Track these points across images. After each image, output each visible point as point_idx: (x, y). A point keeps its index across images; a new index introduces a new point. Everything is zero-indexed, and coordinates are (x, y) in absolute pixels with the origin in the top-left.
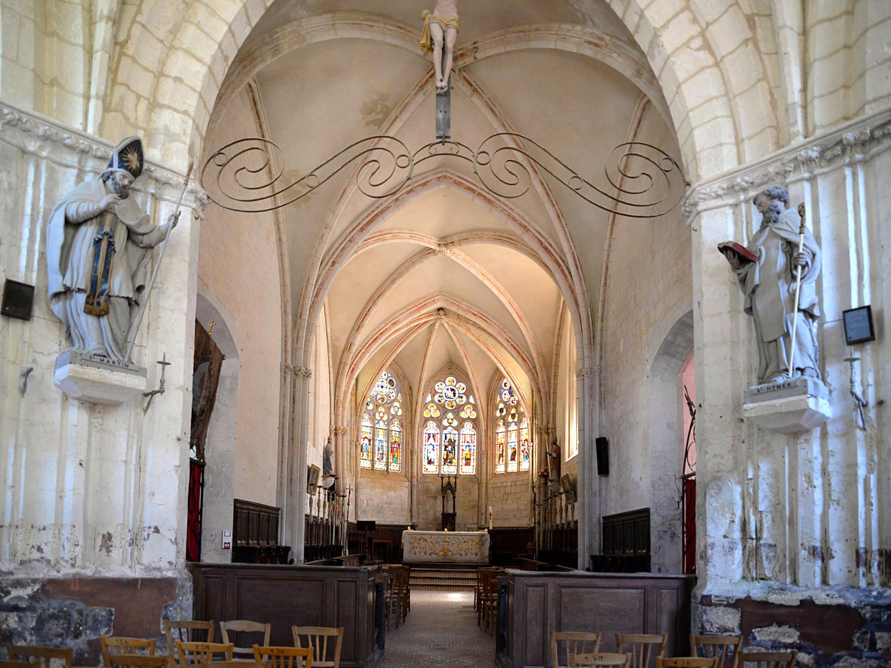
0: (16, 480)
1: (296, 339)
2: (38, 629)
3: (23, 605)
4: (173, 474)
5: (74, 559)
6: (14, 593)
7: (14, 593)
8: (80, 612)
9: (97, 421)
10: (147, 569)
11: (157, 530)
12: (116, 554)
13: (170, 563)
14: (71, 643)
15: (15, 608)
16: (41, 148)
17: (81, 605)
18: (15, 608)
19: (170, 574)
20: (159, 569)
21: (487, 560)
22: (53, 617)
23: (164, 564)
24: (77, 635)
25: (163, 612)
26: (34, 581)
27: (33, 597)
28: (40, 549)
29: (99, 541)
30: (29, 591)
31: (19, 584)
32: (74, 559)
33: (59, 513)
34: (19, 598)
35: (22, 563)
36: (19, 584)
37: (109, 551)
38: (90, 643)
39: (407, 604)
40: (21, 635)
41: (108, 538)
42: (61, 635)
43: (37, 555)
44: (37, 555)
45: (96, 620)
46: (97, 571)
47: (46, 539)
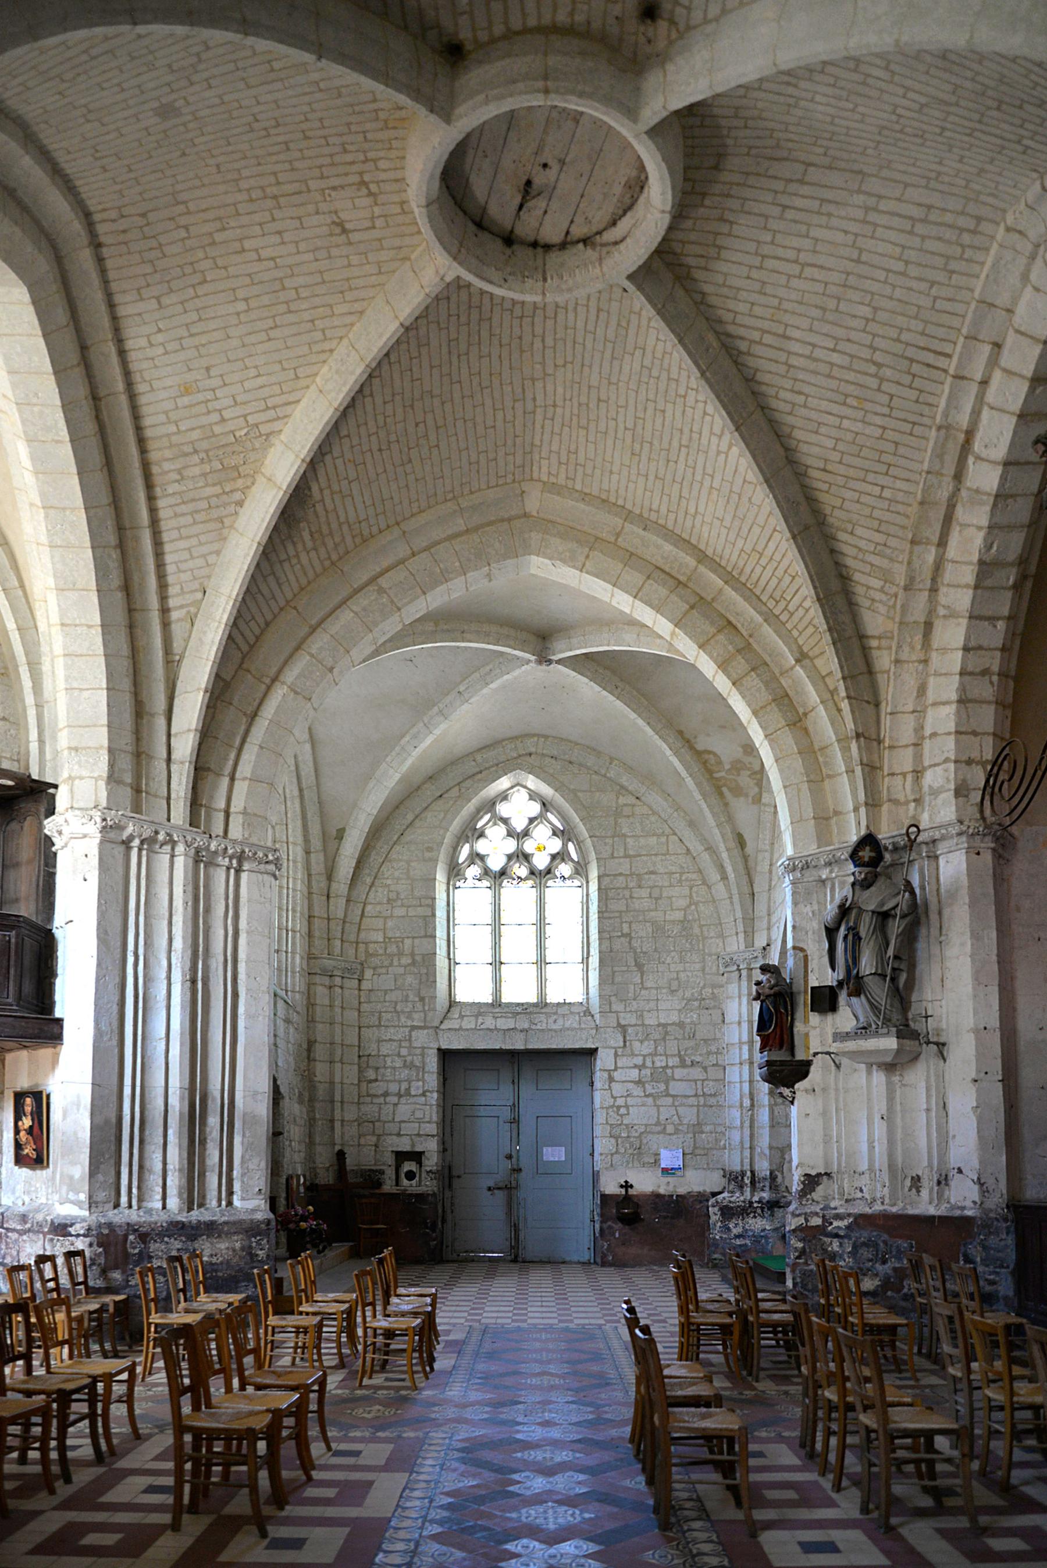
0: (839, 1136)
1: (37, 222)
2: (853, 1253)
3: (842, 1233)
4: (971, 1114)
5: (883, 1198)
6: (836, 1224)
7: (836, 1224)
8: (885, 1242)
9: (896, 1079)
10: (953, 1208)
11: (960, 1171)
12: (925, 1193)
13: (975, 1202)
14: (879, 1267)
15: (837, 1236)
16: (831, 872)
17: (885, 1237)
18: (837, 1236)
19: (969, 1213)
20: (963, 1208)
21: (893, 1426)
22: (864, 1244)
23: (968, 1203)
24: (884, 1262)
25: (962, 1249)
26: (849, 1215)
27: (848, 1227)
28: (861, 1191)
29: (908, 1183)
30: (846, 1222)
31: (839, 1217)
32: (883, 1198)
33: (871, 1161)
34: (839, 1227)
35: (847, 1201)
36: (839, 1217)
37: (918, 1191)
38: (895, 1269)
39: (176, 1460)
40: (841, 1257)
41: (916, 1180)
42: (871, 1260)
43: (859, 1195)
44: (859, 1195)
45: (899, 1251)
46: (904, 1208)
47: (864, 1181)
